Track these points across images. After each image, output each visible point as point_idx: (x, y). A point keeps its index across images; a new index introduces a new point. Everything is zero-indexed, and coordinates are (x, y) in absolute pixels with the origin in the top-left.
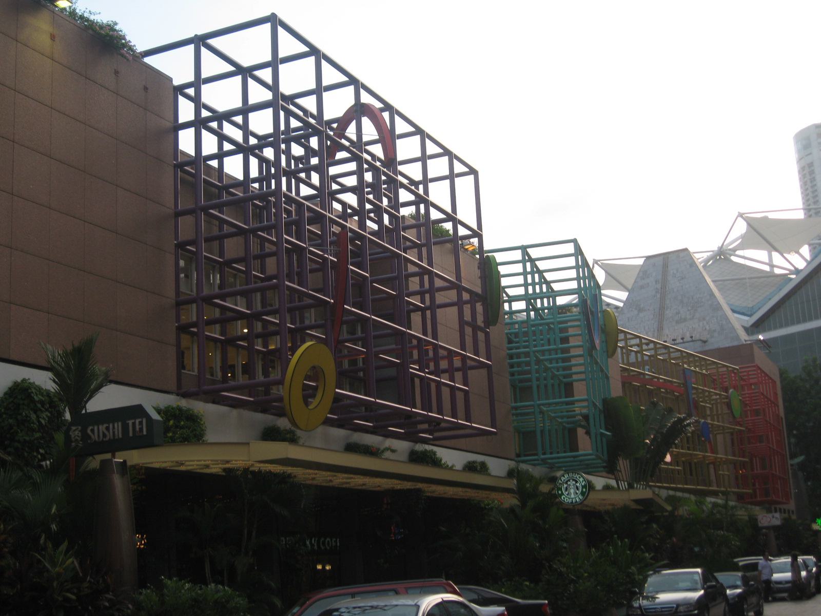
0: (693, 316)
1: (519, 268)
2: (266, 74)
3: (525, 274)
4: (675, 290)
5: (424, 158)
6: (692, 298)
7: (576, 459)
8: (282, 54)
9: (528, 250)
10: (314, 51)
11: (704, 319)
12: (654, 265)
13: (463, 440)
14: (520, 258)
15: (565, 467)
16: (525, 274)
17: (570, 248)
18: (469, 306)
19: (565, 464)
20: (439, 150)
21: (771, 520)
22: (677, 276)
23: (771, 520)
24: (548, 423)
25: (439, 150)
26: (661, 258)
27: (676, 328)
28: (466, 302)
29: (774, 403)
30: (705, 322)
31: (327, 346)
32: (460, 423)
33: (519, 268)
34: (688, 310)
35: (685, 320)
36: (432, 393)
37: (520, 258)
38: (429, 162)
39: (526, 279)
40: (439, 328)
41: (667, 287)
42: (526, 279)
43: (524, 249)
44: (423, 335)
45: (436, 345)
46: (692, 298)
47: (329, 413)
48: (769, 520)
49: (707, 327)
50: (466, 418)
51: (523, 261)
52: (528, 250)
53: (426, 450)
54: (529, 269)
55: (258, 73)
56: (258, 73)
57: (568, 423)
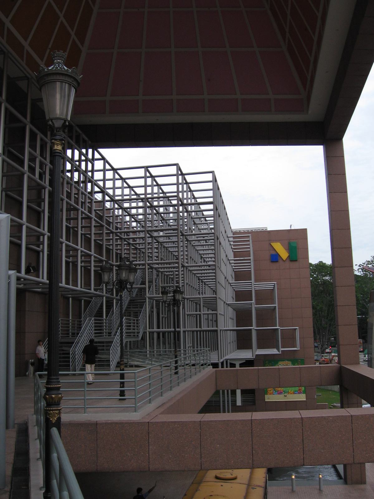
1: (173, 180)
3: (177, 184)
5: (104, 170)
9: (149, 169)
14: (175, 173)
16: (177, 184)
17: (173, 170)
18: (84, 162)
20: (100, 157)
24: (206, 247)
25: (100, 157)
28: (83, 161)
31: (210, 398)
33: (173, 180)
36: (46, 115)
37: (175, 173)
38: (107, 182)
39: (178, 188)
42: (178, 188)
43: (146, 168)
47: (231, 390)
51: (177, 175)
52: (149, 169)
54: (180, 181)
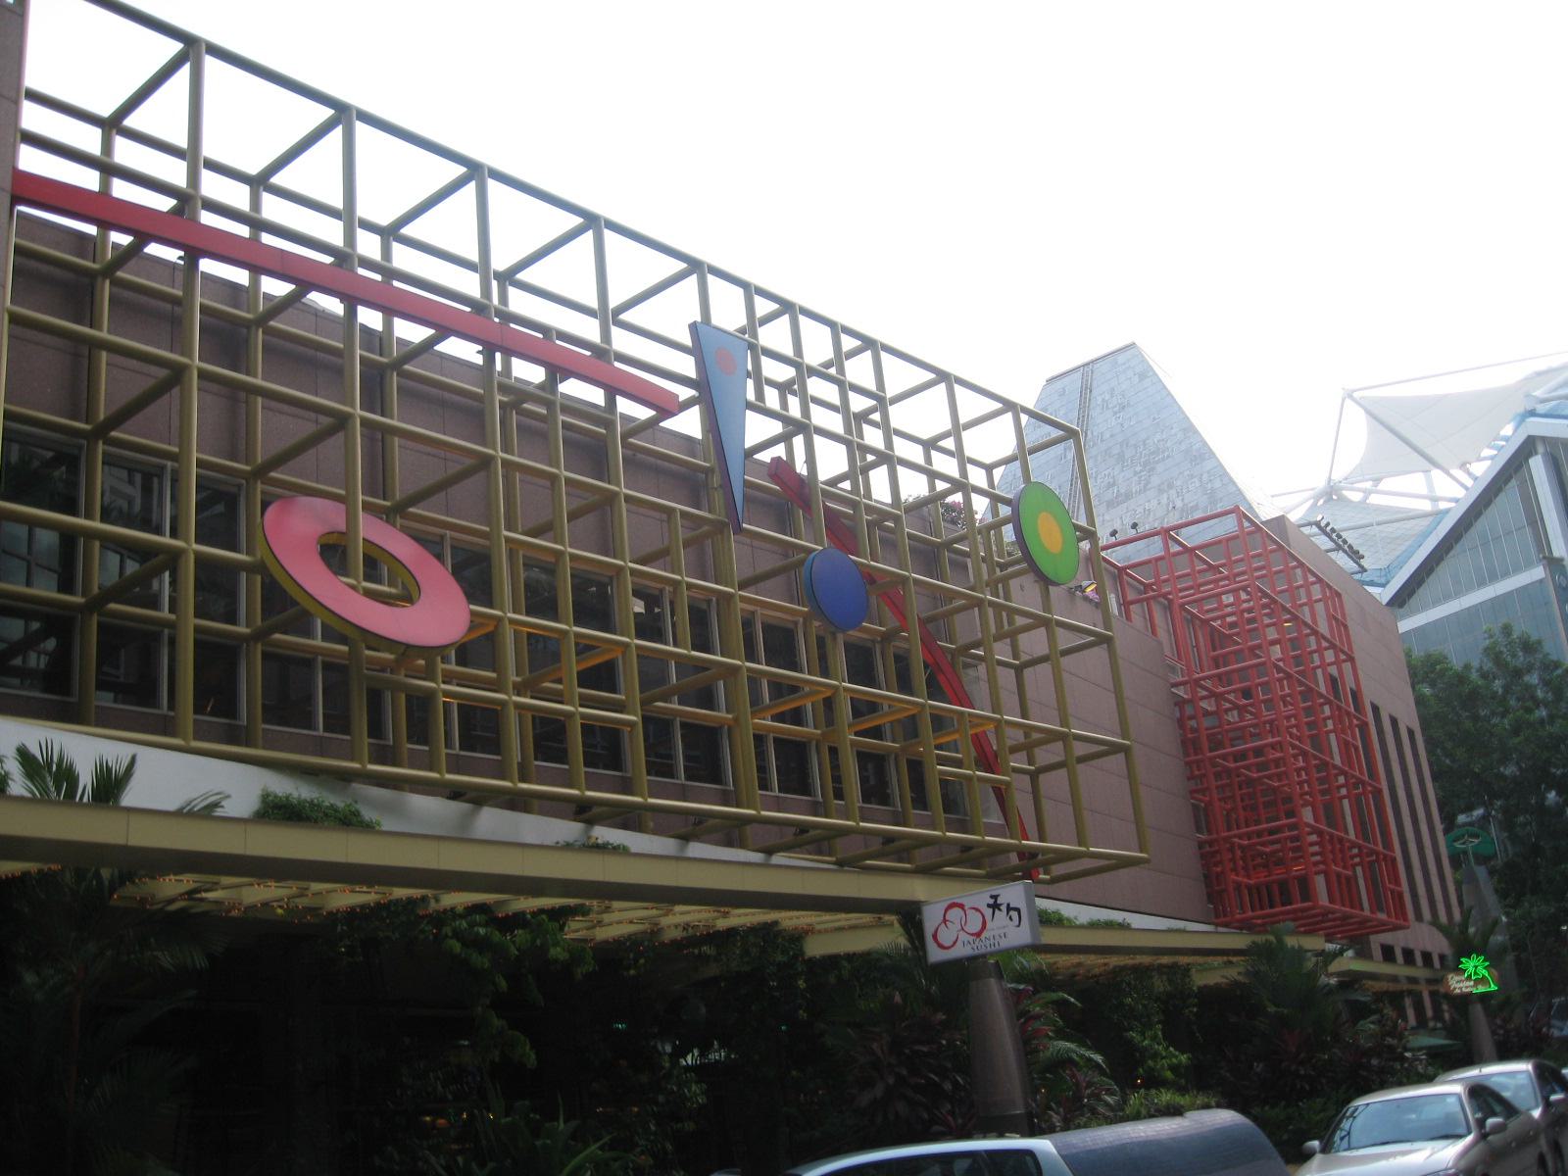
0: (1146, 485)
2: (949, 443)
4: (1107, 435)
6: (1144, 444)
7: (1305, 914)
8: (963, 420)
10: (942, 376)
11: (1170, 486)
12: (1063, 393)
13: (1064, 885)
15: (1340, 932)
19: (1340, 929)
20: (774, 306)
21: (984, 923)
22: (1110, 406)
23: (984, 923)
25: (774, 306)
26: (1078, 375)
27: (1107, 517)
29: (1333, 646)
30: (1173, 492)
32: (950, 838)
34: (1136, 473)
35: (1128, 496)
40: (1030, 704)
41: (1089, 433)
44: (1023, 718)
45: (999, 721)
46: (1144, 444)
48: (974, 925)
49: (1179, 504)
50: (1079, 842)
53: (1300, 947)
55: (942, 443)
56: (942, 443)
57: (1240, 837)
